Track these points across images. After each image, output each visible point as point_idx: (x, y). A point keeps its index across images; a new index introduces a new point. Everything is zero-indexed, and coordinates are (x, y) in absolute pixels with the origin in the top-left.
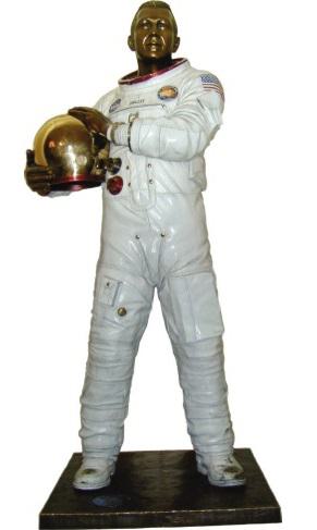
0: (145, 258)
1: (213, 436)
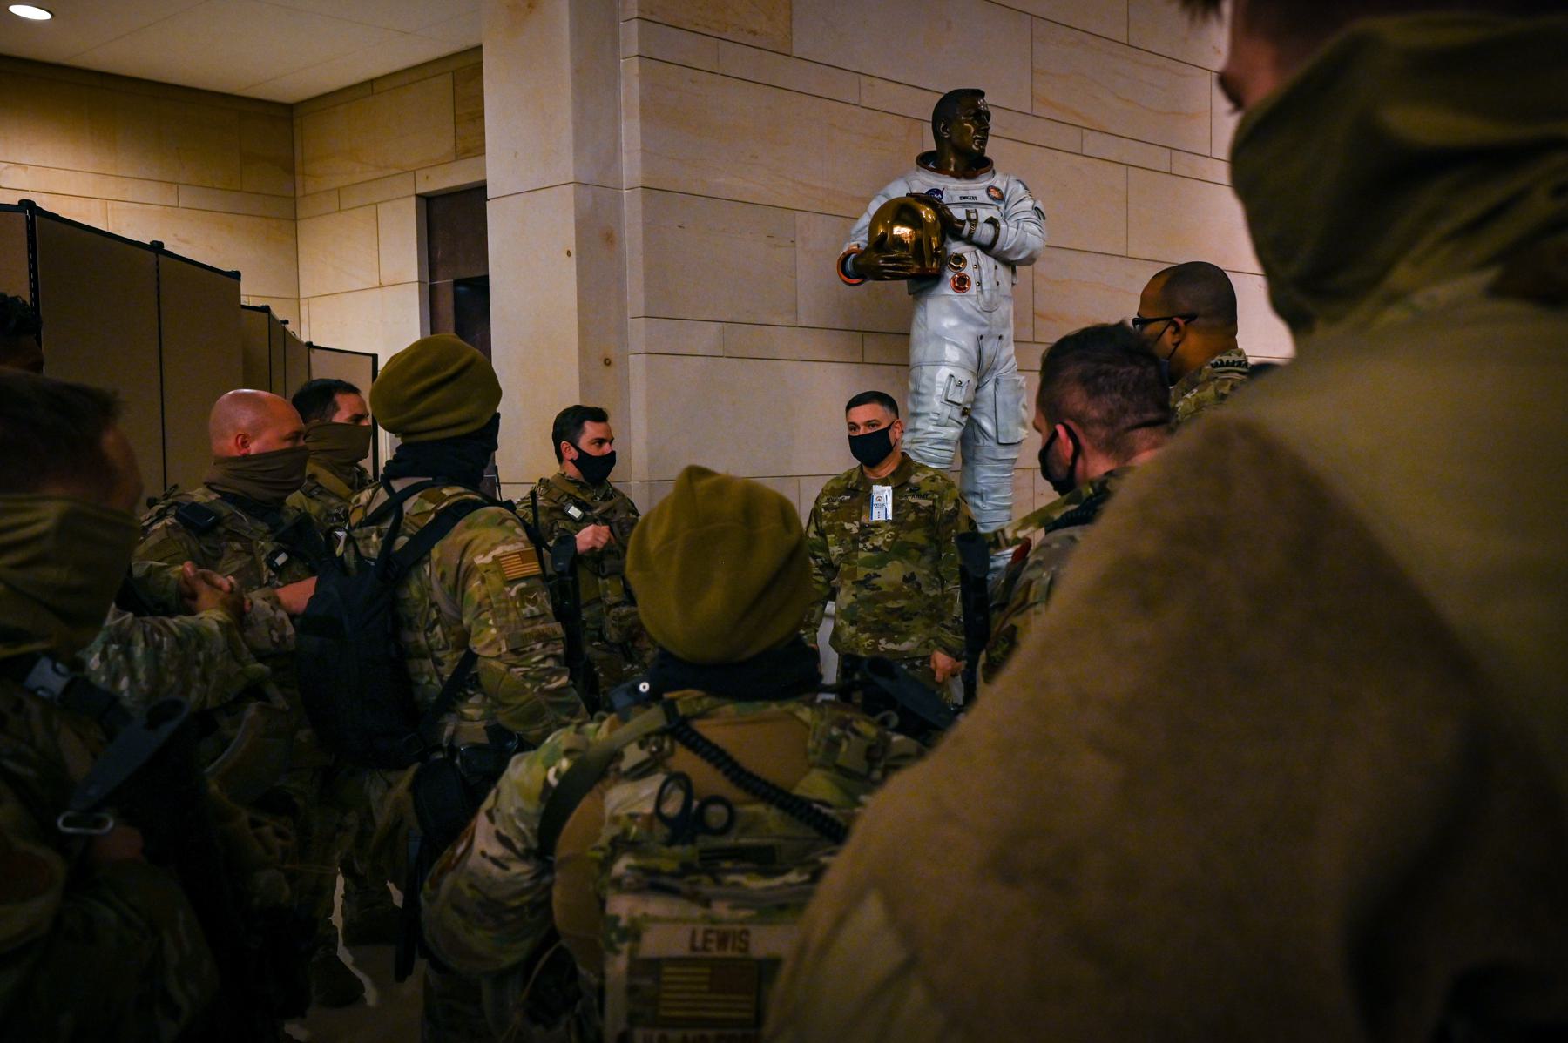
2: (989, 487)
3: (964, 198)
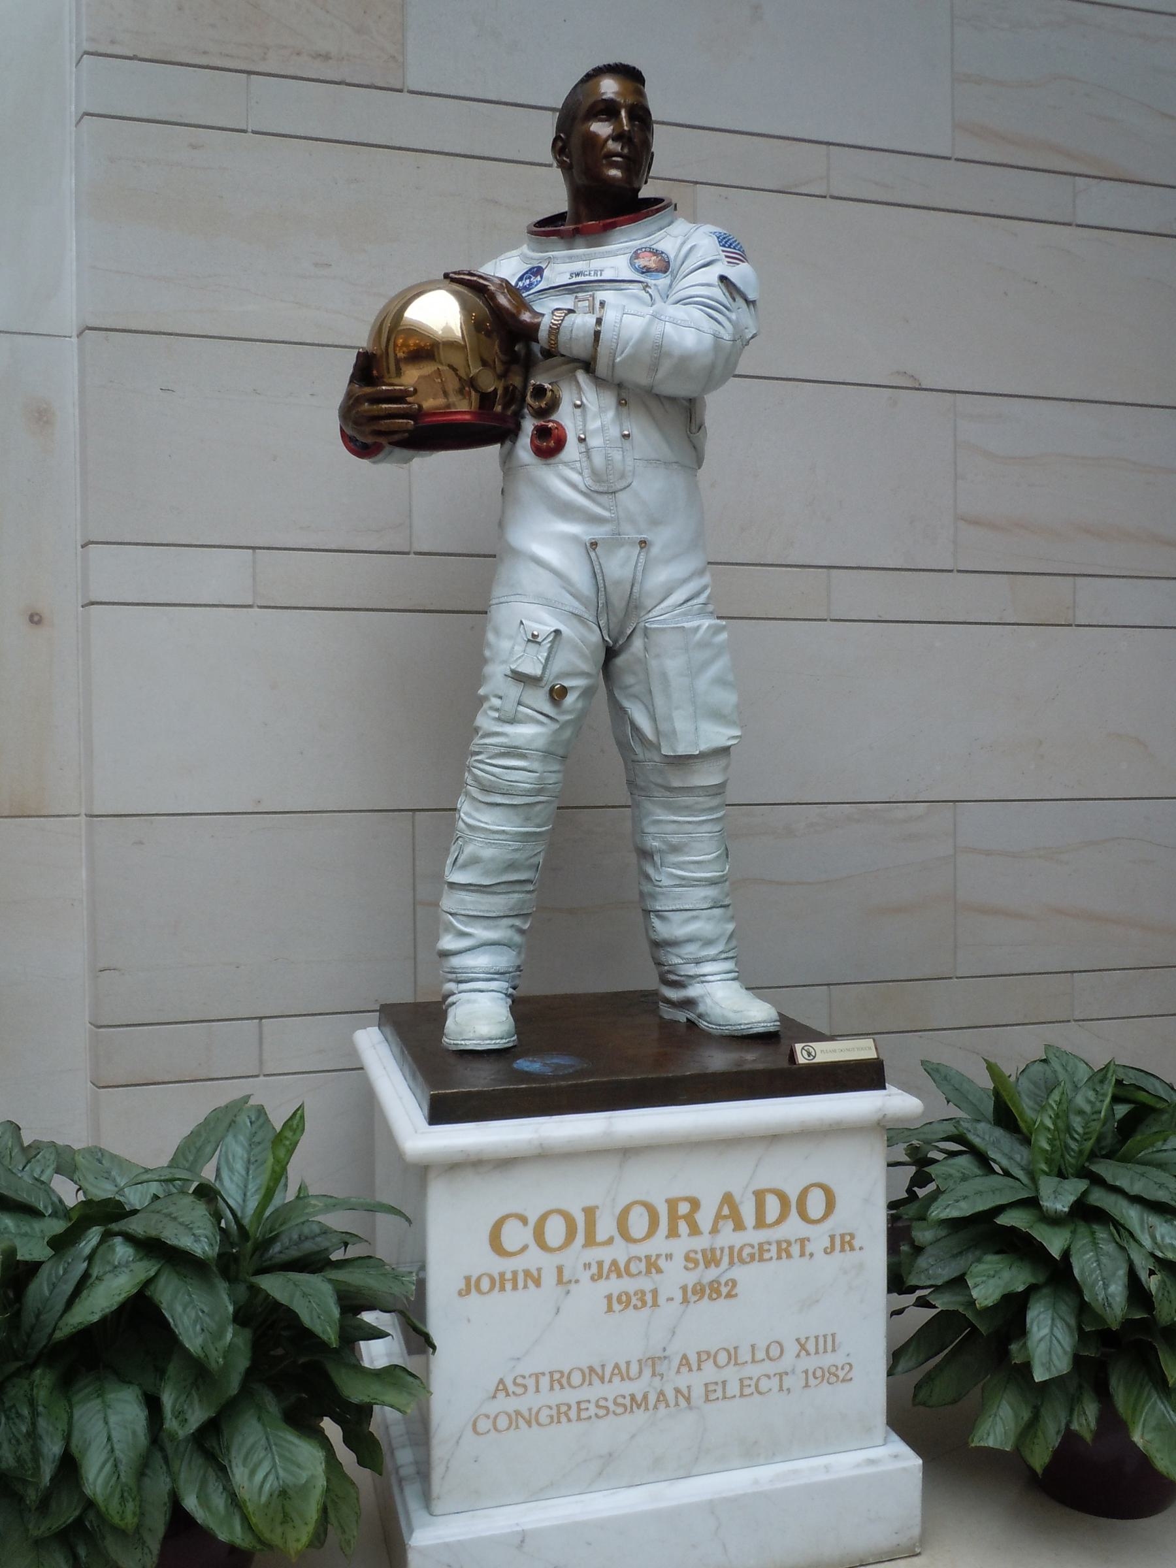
1: (708, 942)
2: (665, 842)
3: (578, 275)
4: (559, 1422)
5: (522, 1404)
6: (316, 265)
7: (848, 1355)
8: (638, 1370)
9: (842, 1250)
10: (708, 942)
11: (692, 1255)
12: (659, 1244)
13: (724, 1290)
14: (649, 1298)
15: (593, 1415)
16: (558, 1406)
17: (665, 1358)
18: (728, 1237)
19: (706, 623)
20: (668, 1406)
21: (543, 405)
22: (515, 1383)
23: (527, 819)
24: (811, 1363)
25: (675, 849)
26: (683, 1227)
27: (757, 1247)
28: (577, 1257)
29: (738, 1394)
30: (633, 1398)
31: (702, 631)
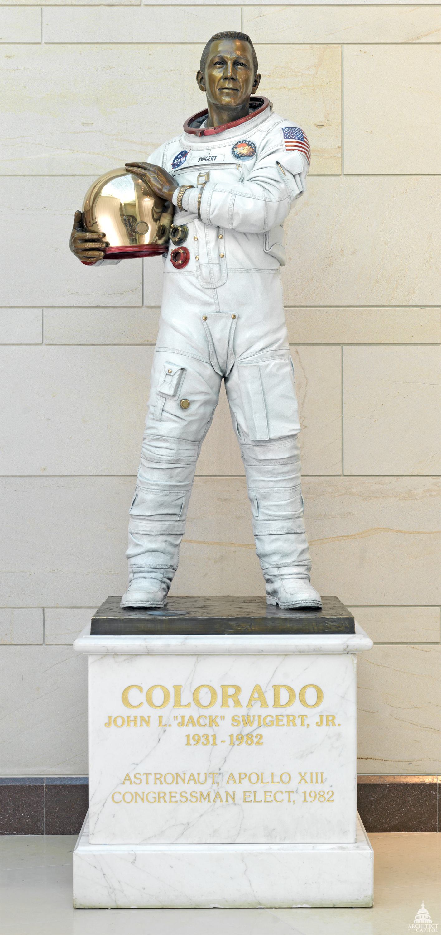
0: (210, 343)
1: (286, 555)
3: (203, 159)
4: (159, 801)
5: (140, 789)
6: (84, 124)
7: (331, 786)
8: (204, 779)
9: (327, 724)
10: (286, 555)
11: (236, 718)
12: (216, 710)
13: (255, 740)
14: (211, 739)
15: (178, 800)
16: (159, 793)
17: (220, 774)
18: (257, 710)
19: (273, 363)
20: (221, 801)
21: (177, 240)
22: (135, 776)
23: (171, 477)
24: (308, 787)
25: (265, 497)
26: (231, 702)
27: (275, 718)
28: (168, 712)
29: (263, 800)
30: (201, 794)
31: (270, 367)
